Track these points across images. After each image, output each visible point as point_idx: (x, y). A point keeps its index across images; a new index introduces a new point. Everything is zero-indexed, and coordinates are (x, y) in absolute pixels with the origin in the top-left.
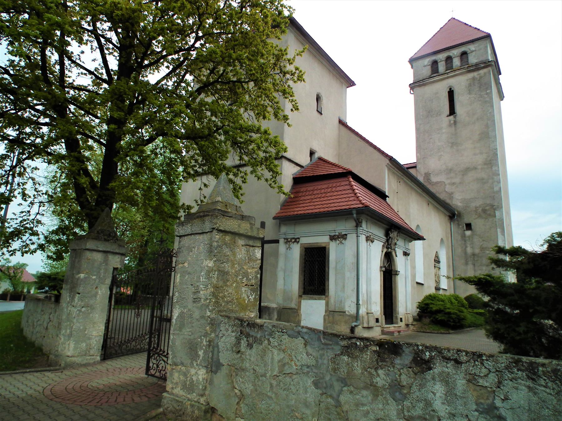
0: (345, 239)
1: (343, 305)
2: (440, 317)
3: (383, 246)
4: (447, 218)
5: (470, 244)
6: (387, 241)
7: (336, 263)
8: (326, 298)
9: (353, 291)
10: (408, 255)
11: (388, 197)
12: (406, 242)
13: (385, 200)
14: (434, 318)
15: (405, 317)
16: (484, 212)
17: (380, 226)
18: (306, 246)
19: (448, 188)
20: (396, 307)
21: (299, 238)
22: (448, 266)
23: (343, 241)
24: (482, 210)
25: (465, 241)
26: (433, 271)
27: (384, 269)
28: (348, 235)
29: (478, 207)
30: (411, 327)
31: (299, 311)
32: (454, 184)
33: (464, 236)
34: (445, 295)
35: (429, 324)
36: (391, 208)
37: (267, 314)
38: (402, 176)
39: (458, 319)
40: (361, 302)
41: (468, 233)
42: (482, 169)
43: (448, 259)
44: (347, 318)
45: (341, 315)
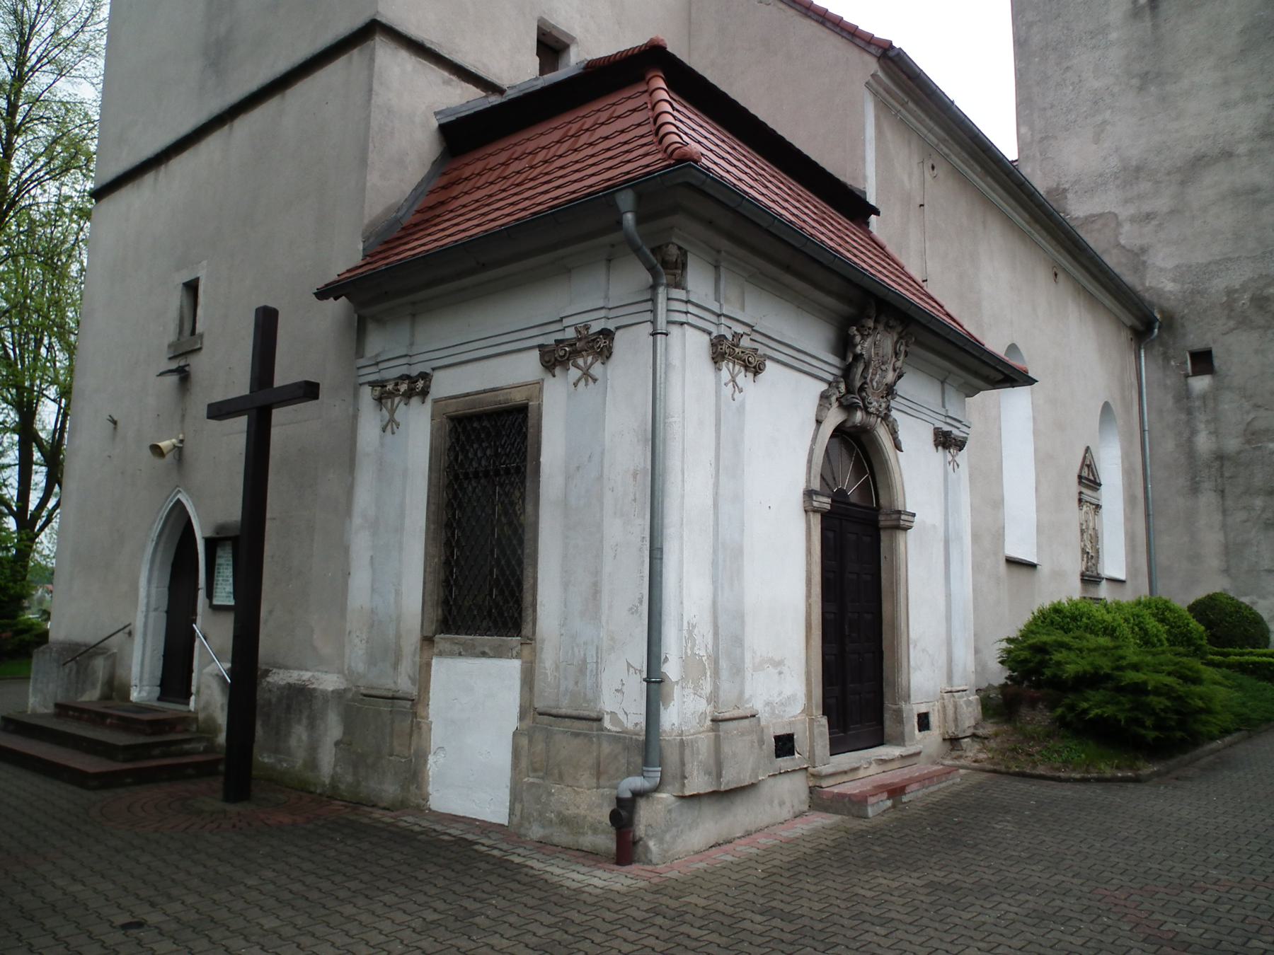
0: (605, 354)
1: (589, 682)
2: (1094, 704)
3: (824, 397)
4: (1125, 335)
5: (1208, 422)
6: (847, 373)
7: (568, 478)
8: (526, 650)
9: (633, 611)
10: (960, 444)
11: (877, 212)
12: (951, 393)
13: (863, 222)
14: (1072, 708)
15: (944, 707)
16: (1261, 308)
17: (802, 303)
18: (452, 409)
19: (1129, 235)
20: (896, 666)
21: (425, 376)
22: (1130, 500)
23: (597, 369)
24: (1253, 299)
25: (1189, 412)
26: (1073, 515)
27: (824, 502)
28: (618, 335)
29: (1236, 291)
30: (972, 750)
31: (420, 709)
32: (1149, 217)
33: (1184, 396)
34: (1119, 607)
35: (1049, 735)
36: (888, 256)
37: (305, 721)
38: (944, 141)
39: (1177, 712)
40: (671, 669)
41: (1201, 383)
42: (1251, 153)
43: (1128, 473)
44: (606, 748)
45: (577, 735)
